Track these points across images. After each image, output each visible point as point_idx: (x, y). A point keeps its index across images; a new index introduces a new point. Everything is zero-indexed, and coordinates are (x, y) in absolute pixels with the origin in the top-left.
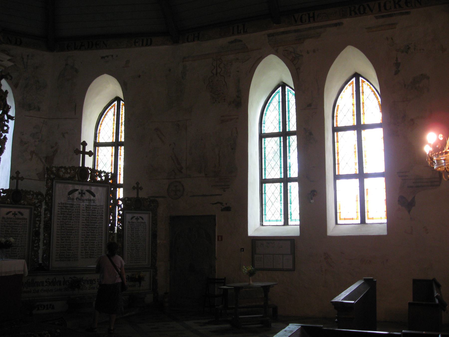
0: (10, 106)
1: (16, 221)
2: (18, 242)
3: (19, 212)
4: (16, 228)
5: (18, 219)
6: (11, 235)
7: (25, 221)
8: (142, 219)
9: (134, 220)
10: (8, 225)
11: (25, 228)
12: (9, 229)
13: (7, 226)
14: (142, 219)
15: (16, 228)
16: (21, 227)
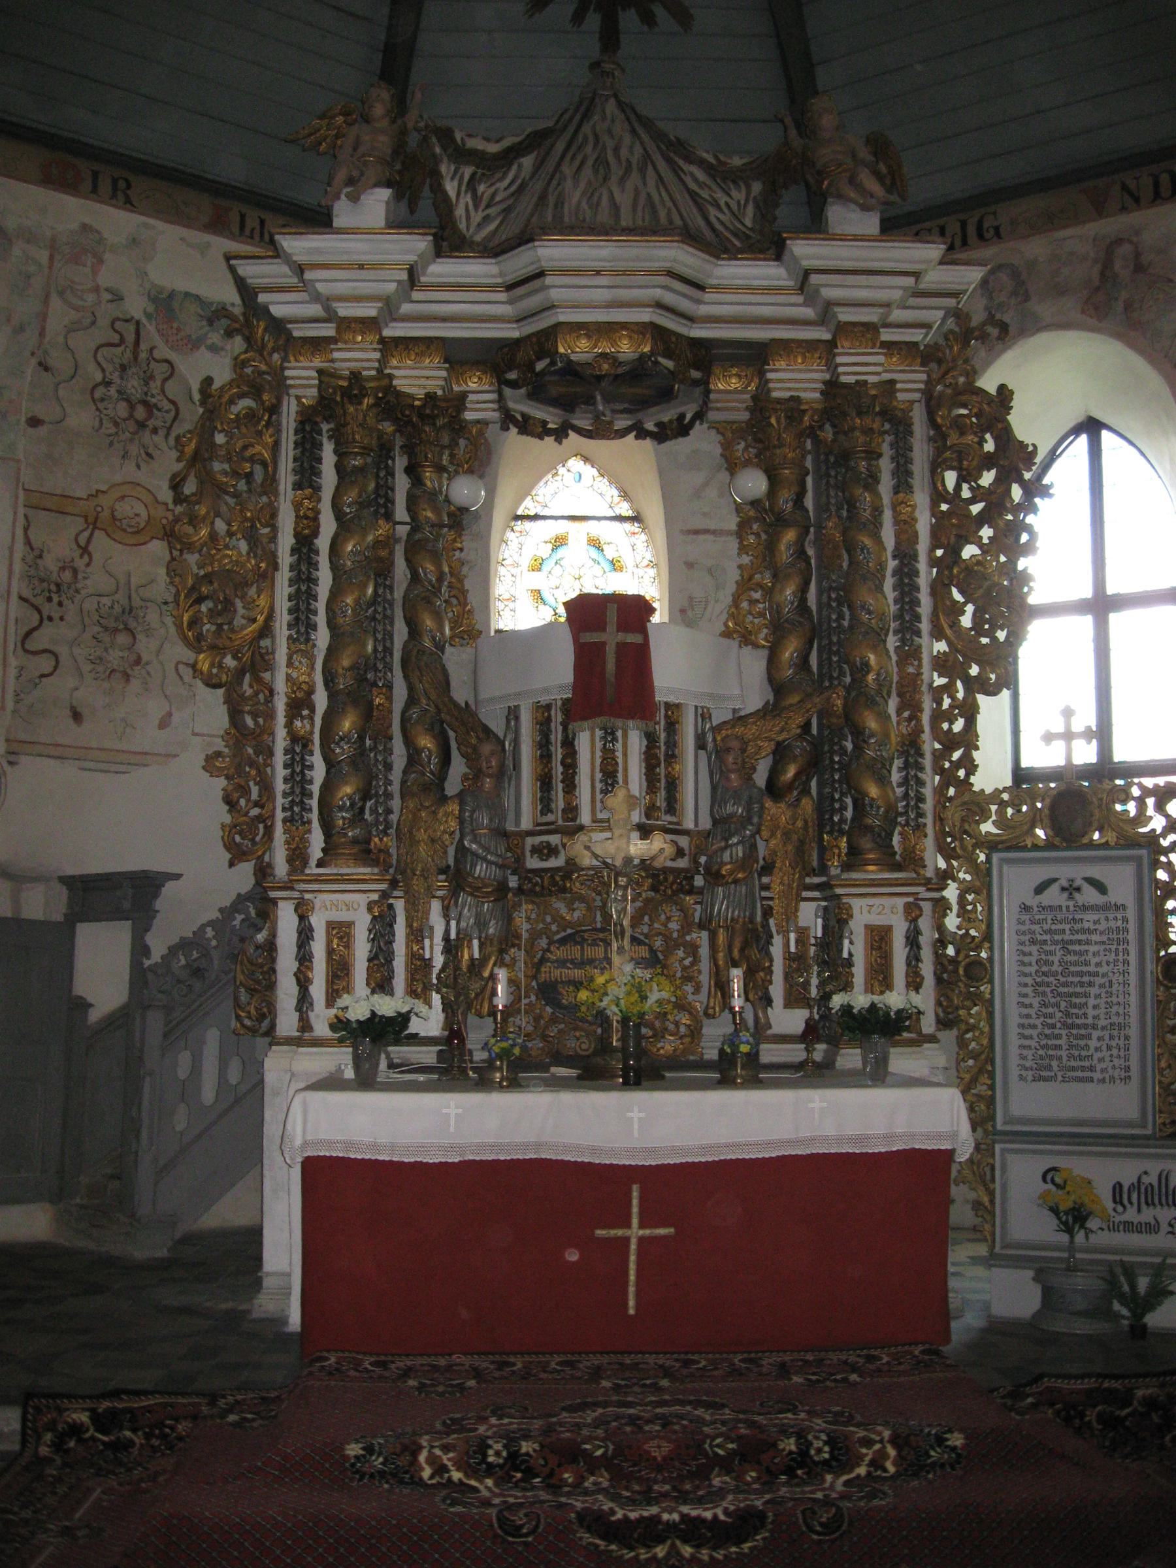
0: (1033, 445)
1: (1077, 917)
2: (1095, 1007)
3: (1091, 881)
4: (1083, 948)
5: (1085, 908)
6: (1063, 979)
7: (1119, 917)
8: (1101, 888)
9: (1052, 896)
10: (1047, 937)
11: (1120, 948)
12: (1052, 953)
13: (1045, 942)
14: (1101, 888)
15: (1083, 948)
16: (1104, 943)
